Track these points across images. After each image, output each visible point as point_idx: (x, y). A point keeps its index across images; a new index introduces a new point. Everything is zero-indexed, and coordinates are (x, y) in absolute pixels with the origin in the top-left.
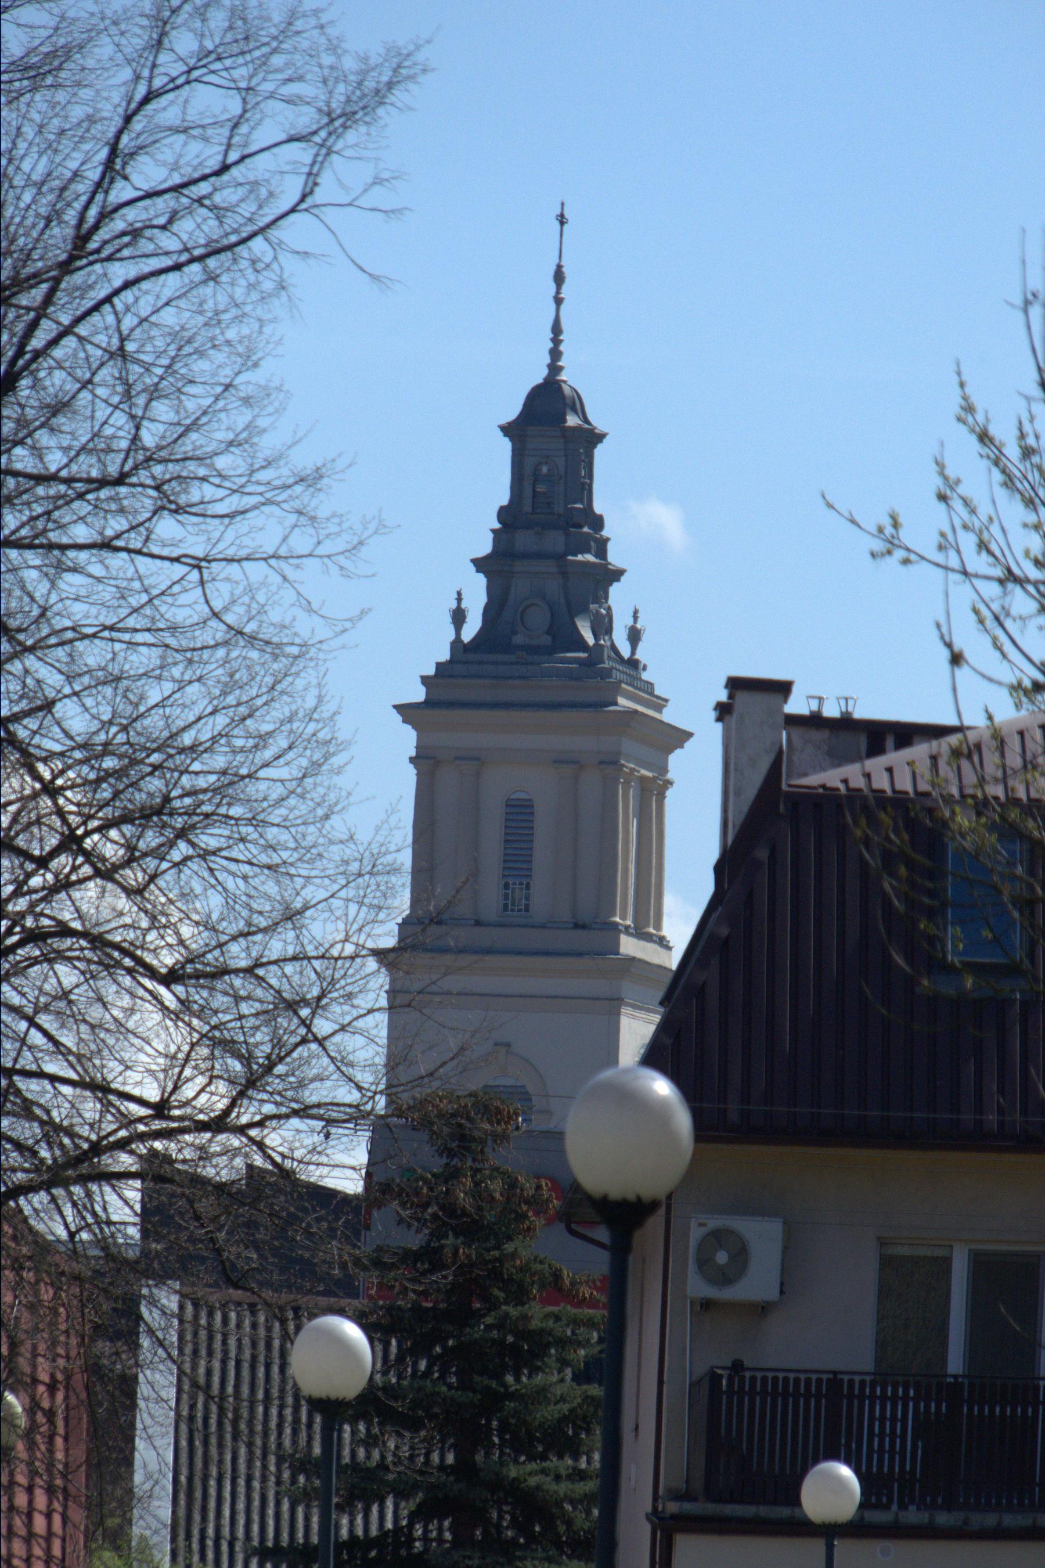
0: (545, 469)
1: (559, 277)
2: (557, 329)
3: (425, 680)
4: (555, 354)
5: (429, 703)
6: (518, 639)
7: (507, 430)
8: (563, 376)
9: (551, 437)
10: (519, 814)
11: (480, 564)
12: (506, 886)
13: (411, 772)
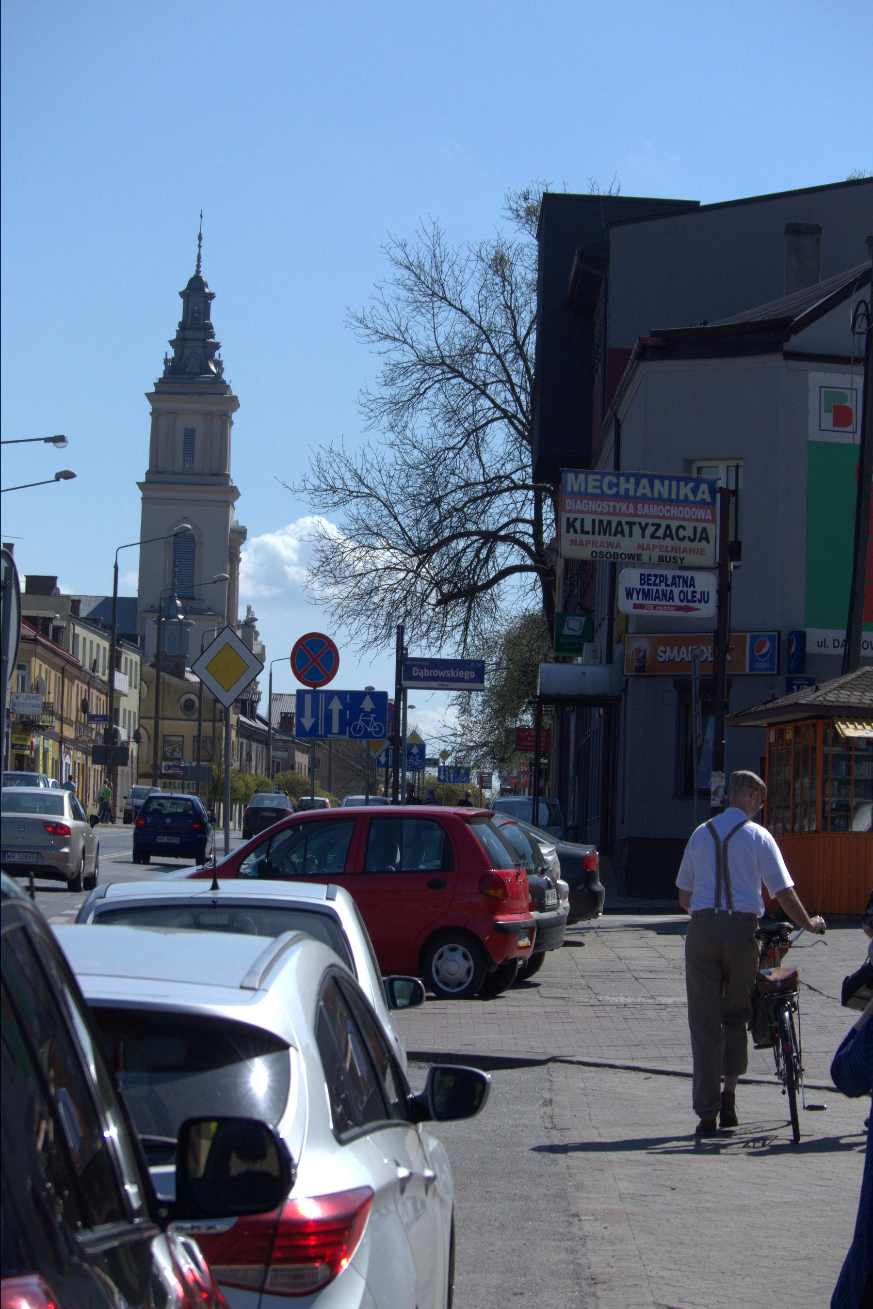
1: (200, 238)
2: (199, 257)
3: (155, 384)
4: (198, 266)
5: (156, 393)
6: (187, 370)
7: (182, 294)
9: (196, 296)
10: (190, 434)
11: (172, 343)
13: (150, 418)
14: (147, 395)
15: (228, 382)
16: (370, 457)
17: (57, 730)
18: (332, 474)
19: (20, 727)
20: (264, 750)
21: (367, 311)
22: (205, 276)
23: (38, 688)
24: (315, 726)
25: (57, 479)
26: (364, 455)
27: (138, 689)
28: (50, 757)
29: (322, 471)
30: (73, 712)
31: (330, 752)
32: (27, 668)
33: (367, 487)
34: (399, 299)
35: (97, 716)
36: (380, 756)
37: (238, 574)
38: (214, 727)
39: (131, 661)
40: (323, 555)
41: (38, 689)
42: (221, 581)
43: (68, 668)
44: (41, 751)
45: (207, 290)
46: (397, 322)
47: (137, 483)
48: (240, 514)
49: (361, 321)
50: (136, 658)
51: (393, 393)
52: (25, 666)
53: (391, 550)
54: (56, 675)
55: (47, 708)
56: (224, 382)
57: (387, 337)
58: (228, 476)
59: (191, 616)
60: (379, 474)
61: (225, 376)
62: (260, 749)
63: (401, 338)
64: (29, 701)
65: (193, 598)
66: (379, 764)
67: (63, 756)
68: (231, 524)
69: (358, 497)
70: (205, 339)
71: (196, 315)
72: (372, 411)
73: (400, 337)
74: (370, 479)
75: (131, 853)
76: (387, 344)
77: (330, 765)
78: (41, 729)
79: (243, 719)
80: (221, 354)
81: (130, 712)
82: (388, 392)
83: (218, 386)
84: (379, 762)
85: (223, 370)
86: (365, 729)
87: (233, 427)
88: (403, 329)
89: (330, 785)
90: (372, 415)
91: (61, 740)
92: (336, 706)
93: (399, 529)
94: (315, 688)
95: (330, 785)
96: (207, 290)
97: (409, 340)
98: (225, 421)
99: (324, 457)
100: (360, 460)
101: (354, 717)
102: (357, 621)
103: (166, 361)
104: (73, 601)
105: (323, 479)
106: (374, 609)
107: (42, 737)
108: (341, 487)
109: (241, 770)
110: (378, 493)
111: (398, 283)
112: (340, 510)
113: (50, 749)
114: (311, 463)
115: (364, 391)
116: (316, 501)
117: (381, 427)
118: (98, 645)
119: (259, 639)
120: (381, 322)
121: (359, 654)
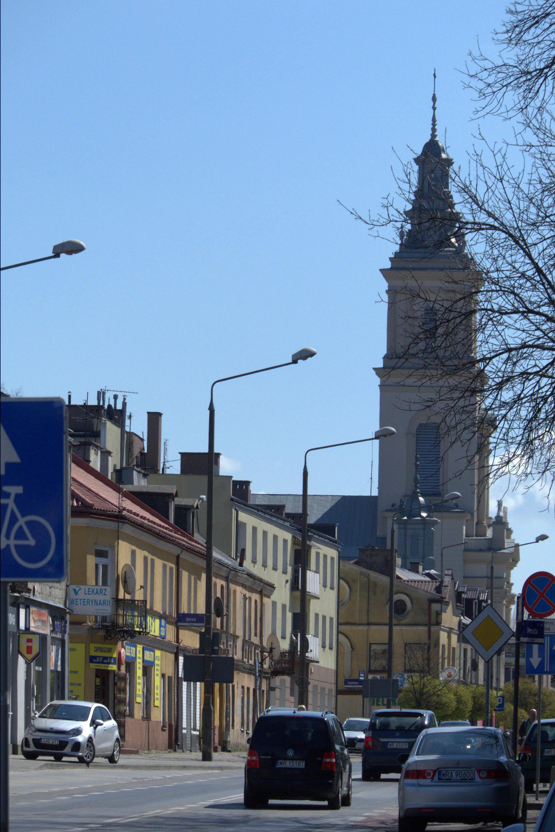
1: (434, 99)
2: (434, 120)
3: (391, 259)
4: (434, 130)
8: (437, 139)
14: (382, 271)
19: (102, 633)
22: (440, 140)
25: (57, 255)
32: (109, 555)
33: (490, 214)
35: (189, 615)
38: (429, 632)
39: (325, 556)
43: (185, 556)
45: (444, 156)
47: (374, 369)
50: (332, 553)
52: (107, 552)
54: (165, 567)
59: (435, 514)
64: (92, 597)
78: (130, 635)
81: (324, 617)
82: (511, 55)
96: (444, 156)
104: (236, 483)
107: (140, 648)
113: (157, 662)
115: (476, 54)
118: (275, 537)
119: (513, 536)
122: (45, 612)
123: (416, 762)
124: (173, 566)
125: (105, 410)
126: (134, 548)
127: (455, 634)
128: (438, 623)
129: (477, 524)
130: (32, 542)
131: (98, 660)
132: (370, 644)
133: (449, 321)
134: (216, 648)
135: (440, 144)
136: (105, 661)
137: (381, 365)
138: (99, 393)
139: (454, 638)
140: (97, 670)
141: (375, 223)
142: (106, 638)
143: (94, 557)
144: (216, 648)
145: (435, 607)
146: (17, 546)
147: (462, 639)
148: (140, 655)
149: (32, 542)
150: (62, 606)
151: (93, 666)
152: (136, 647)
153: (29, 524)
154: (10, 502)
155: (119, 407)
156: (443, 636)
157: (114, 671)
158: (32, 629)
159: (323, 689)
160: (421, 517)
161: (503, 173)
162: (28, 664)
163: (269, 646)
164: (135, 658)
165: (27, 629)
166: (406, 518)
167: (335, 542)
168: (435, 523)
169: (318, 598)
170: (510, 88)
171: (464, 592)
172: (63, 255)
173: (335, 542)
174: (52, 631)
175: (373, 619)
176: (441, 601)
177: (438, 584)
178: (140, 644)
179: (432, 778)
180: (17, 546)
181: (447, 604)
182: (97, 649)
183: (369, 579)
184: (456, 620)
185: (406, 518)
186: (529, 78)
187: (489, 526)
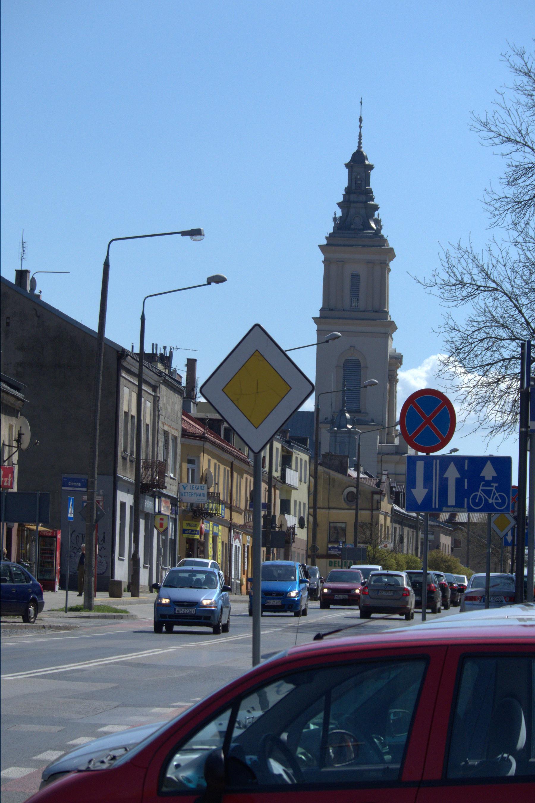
0: (359, 177)
1: (361, 120)
2: (360, 136)
3: (326, 238)
4: (360, 143)
6: (353, 227)
7: (347, 165)
8: (362, 150)
9: (359, 167)
10: (355, 278)
11: (339, 204)
12: (351, 299)
13: (322, 266)
15: (385, 237)
16: (496, 252)
17: (227, 517)
18: (460, 269)
19: (191, 514)
20: (415, 533)
21: (490, 115)
22: (365, 151)
23: (206, 479)
24: (428, 499)
25: (209, 283)
26: (490, 251)
27: (307, 483)
28: (220, 541)
29: (451, 267)
30: (242, 499)
31: (468, 533)
33: (494, 281)
34: (519, 103)
36: (507, 535)
37: (396, 392)
38: (372, 513)
39: (301, 460)
40: (453, 345)
41: (206, 480)
42: (371, 385)
43: (237, 463)
44: (211, 536)
45: (367, 162)
46: (519, 126)
47: (313, 318)
48: (397, 343)
49: (485, 125)
50: (305, 457)
51: (516, 192)
52: (194, 460)
53: (517, 341)
54: (225, 469)
55: (214, 497)
56: (382, 236)
57: (509, 140)
58: (387, 313)
59: (357, 426)
60: (503, 268)
61: (383, 232)
62: (410, 533)
63: (522, 141)
64: (194, 491)
65: (360, 412)
66: (506, 543)
67: (233, 539)
68: (390, 351)
69: (485, 291)
70: (366, 202)
71: (359, 182)
72: (496, 209)
73: (520, 141)
74: (496, 274)
75: (262, 633)
76: (509, 147)
77: (468, 545)
78: (209, 516)
79: (396, 508)
80: (379, 214)
81: (300, 503)
82: (510, 192)
83: (378, 240)
84: (506, 541)
85: (381, 227)
86: (486, 501)
87: (390, 273)
88: (524, 132)
89: (468, 562)
90: (497, 212)
91: (231, 526)
92: (452, 474)
93: (523, 320)
94: (428, 454)
95: (468, 562)
97: (529, 144)
98: (384, 268)
99: (453, 253)
100: (486, 254)
101: (474, 487)
102: (485, 408)
103: (335, 219)
105: (452, 275)
106: (501, 397)
107: (211, 524)
108: (469, 281)
109: (394, 550)
110: (503, 287)
111: (518, 88)
112: (469, 303)
113: (220, 534)
114: (441, 260)
115: (489, 190)
116: (446, 295)
117: (505, 224)
120: (503, 126)
121: (487, 439)
122: (169, 501)
123: (472, 592)
124: (229, 469)
125: (158, 357)
126: (210, 457)
127: (389, 516)
128: (378, 509)
129: (387, 434)
130: (500, 501)
131: (188, 532)
132: (330, 522)
133: (471, 344)
134: (274, 525)
135: (364, 154)
136: (192, 533)
137: (318, 315)
138: (153, 344)
139: (389, 519)
140: (187, 539)
141: (428, 285)
142: (193, 518)
143: (186, 464)
144: (274, 525)
145: (376, 497)
146: (495, 503)
147: (393, 521)
148: (211, 529)
149: (500, 501)
150: (175, 496)
151: (185, 536)
152: (209, 523)
153: (500, 495)
154: (494, 489)
155: (168, 355)
156: (382, 517)
157: (198, 539)
158: (162, 512)
159: (299, 554)
160: (348, 428)
161: (506, 261)
162: (159, 534)
163: (280, 523)
164: (209, 531)
165: (160, 512)
166: (336, 429)
167: (308, 450)
168: (357, 433)
169: (297, 489)
170: (509, 211)
171: (394, 487)
172: (213, 284)
173: (308, 450)
174: (171, 513)
175: (332, 505)
176: (380, 493)
177: (378, 481)
178: (212, 521)
179: (480, 601)
180: (495, 503)
181: (384, 495)
182: (188, 525)
183: (330, 476)
184: (390, 506)
185: (336, 429)
186: (520, 205)
187: (396, 436)
